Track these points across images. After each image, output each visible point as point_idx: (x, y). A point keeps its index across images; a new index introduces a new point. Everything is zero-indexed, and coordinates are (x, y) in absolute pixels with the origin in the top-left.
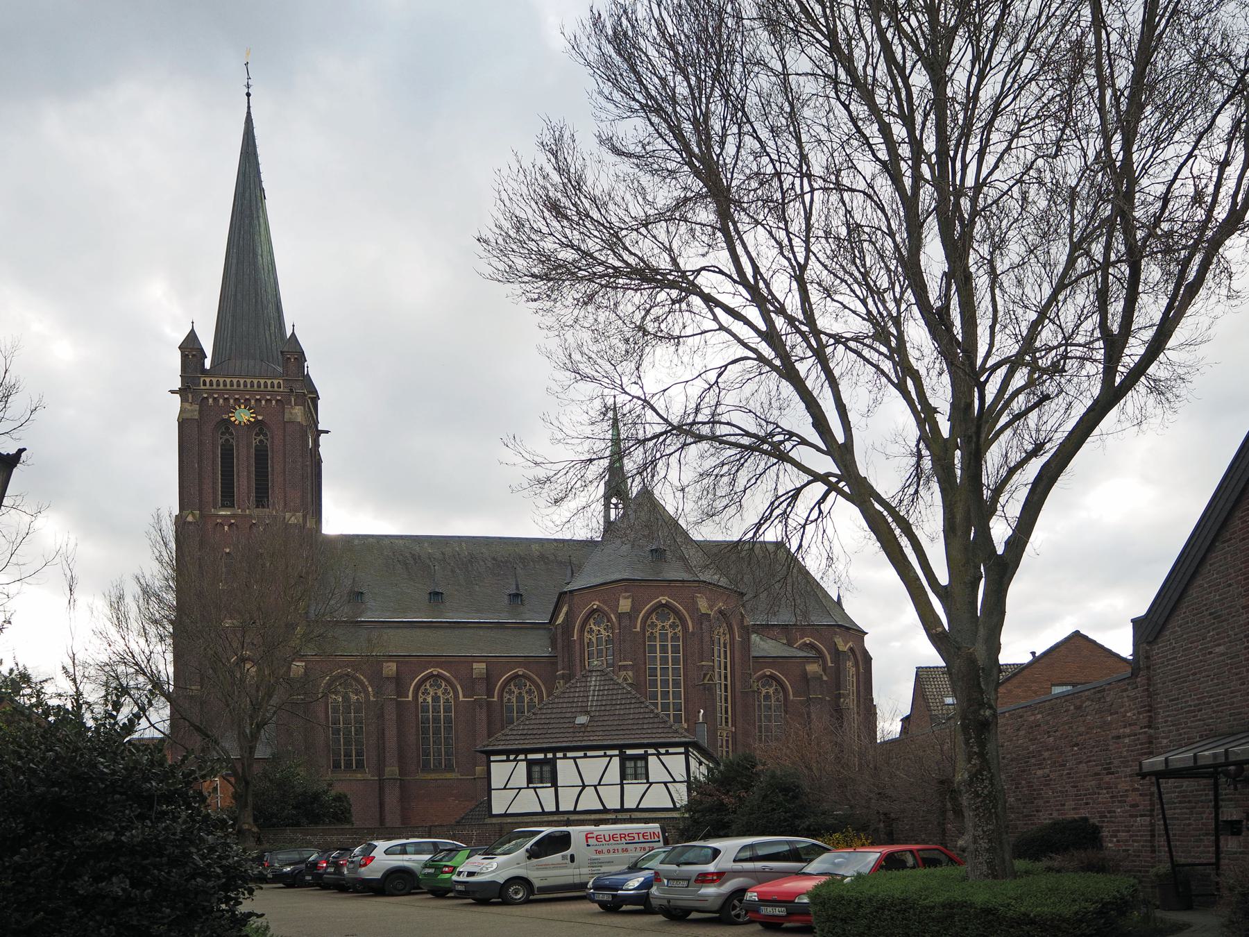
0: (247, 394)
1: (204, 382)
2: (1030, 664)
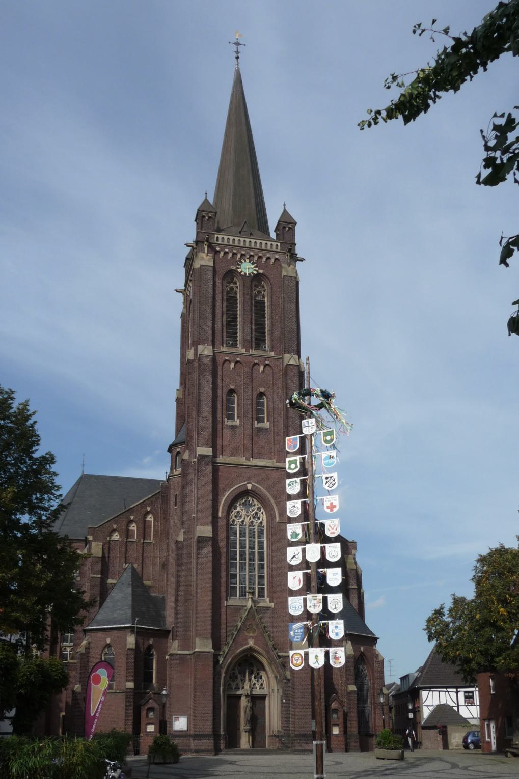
0: (244, 250)
1: (218, 238)
2: (13, 726)
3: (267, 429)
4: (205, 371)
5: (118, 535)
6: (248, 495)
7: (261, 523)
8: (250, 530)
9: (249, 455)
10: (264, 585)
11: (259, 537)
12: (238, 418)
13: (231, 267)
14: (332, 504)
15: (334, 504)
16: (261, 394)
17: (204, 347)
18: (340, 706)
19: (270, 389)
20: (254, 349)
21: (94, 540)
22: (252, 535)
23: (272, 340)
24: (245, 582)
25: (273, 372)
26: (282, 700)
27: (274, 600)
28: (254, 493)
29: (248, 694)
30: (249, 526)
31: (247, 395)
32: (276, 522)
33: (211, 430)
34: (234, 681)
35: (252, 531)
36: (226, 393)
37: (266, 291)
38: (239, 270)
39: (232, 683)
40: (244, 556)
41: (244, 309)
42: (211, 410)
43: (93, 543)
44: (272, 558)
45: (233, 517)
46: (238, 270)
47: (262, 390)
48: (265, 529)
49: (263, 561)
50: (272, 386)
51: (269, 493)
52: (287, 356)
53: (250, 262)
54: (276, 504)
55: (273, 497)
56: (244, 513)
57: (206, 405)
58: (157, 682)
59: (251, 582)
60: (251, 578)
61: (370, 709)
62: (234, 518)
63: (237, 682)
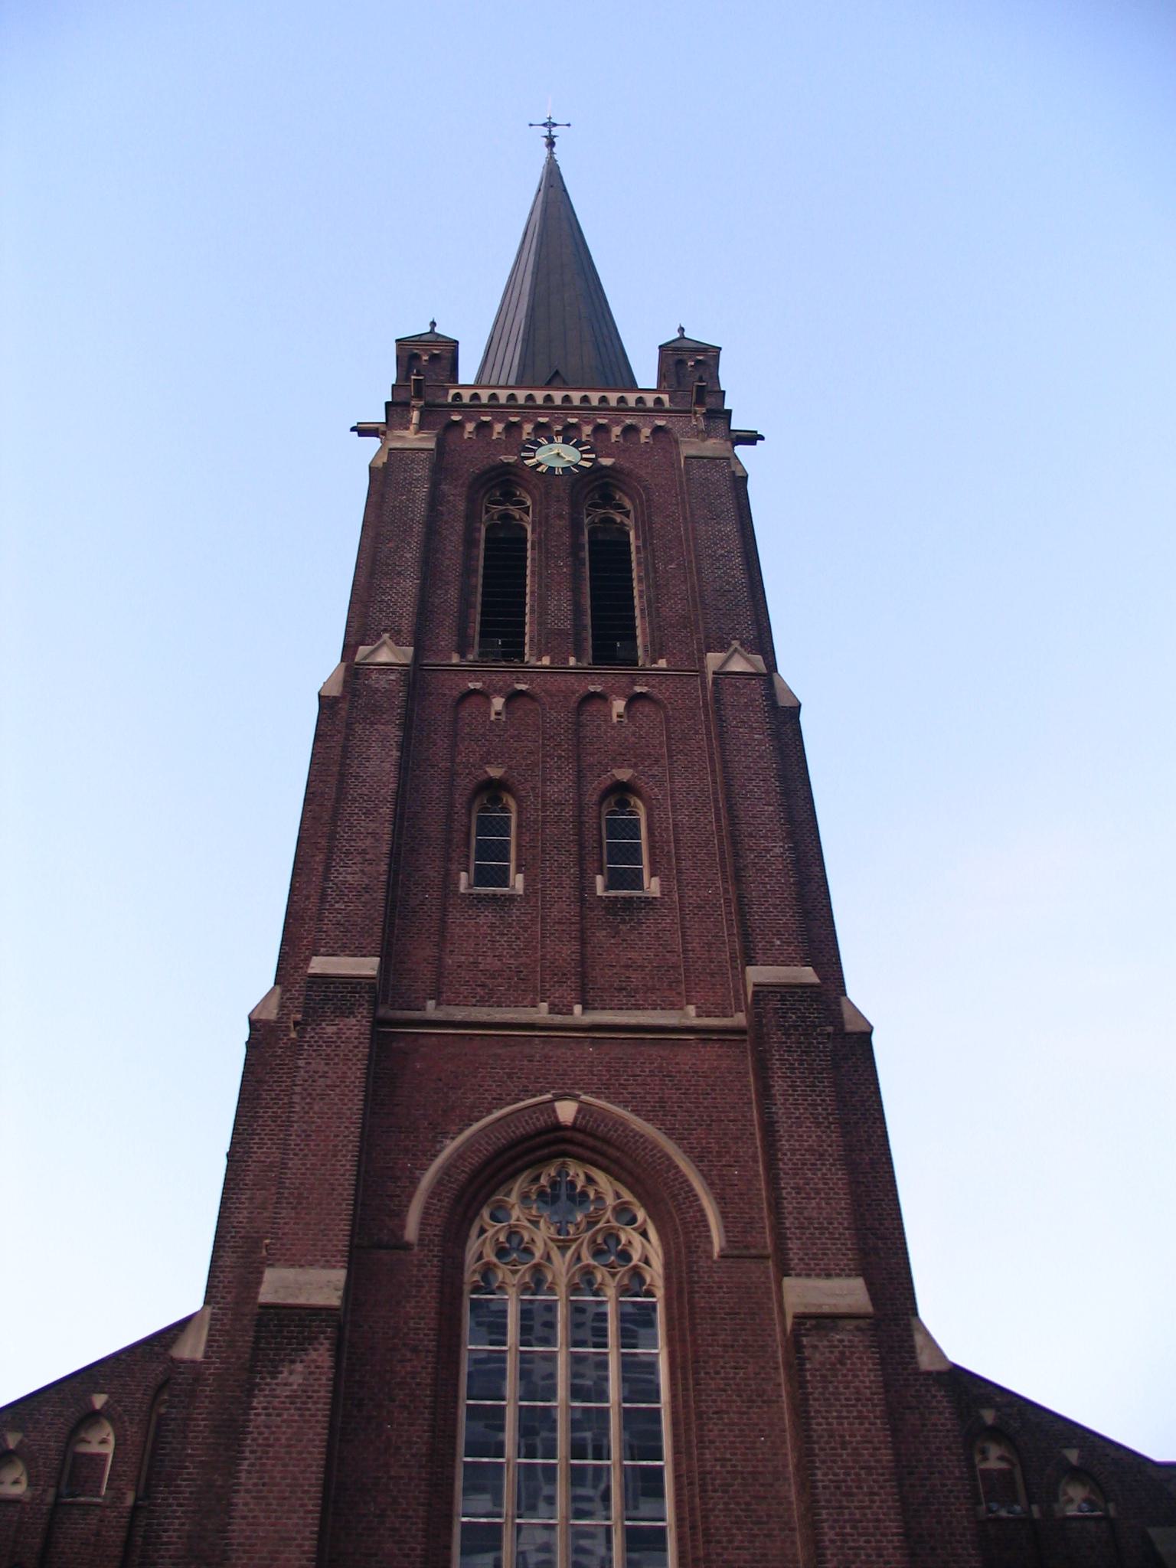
3: (649, 902)
5: (24, 1479)
6: (564, 1154)
8: (577, 1309)
11: (628, 1338)
12: (518, 871)
13: (502, 457)
16: (621, 792)
28: (590, 1141)
30: (574, 1289)
31: (560, 788)
32: (710, 1257)
33: (380, 895)
35: (588, 1317)
37: (632, 514)
40: (544, 1434)
42: (388, 828)
46: (527, 462)
47: (624, 774)
48: (659, 1298)
50: (665, 762)
51: (670, 1133)
54: (705, 1177)
55: (688, 1151)
56: (541, 1236)
57: (368, 813)
60: (583, 1542)
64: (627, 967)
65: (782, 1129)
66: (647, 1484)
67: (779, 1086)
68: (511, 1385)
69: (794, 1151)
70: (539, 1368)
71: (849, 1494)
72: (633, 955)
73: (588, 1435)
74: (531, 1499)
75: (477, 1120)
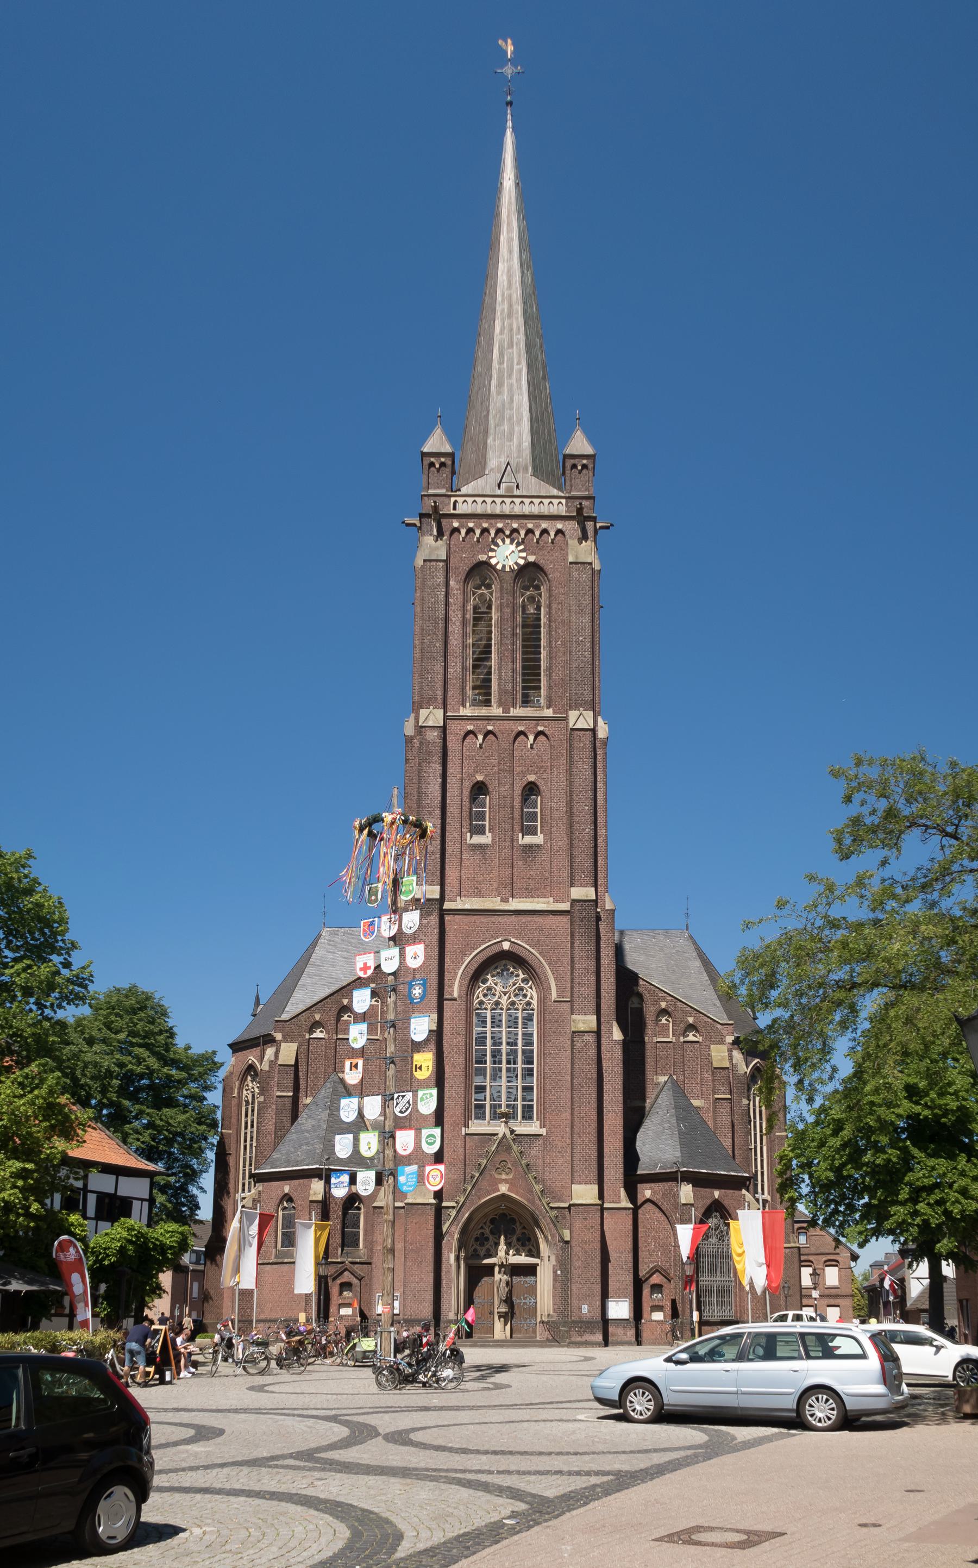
3: (538, 846)
4: (429, 755)
7: (529, 1004)
9: (506, 892)
10: (532, 1101)
11: (525, 1025)
14: (365, 964)
15: (368, 965)
17: (428, 711)
18: (665, 1280)
19: (545, 775)
20: (518, 706)
21: (285, 1039)
22: (513, 1023)
23: (550, 688)
24: (500, 1097)
25: (551, 745)
26: (555, 1272)
27: (547, 1123)
29: (502, 1263)
34: (482, 1245)
35: (513, 1017)
36: (469, 789)
38: (493, 561)
39: (478, 1248)
40: (498, 1057)
41: (501, 634)
43: (283, 1045)
44: (544, 1059)
45: (481, 995)
49: (532, 1063)
52: (573, 715)
53: (511, 543)
58: (365, 1247)
59: (511, 1096)
60: (510, 1090)
61: (733, 1284)
62: (482, 998)
63: (487, 1247)
64: (529, 878)
65: (576, 959)
66: (529, 1073)
67: (577, 943)
68: (489, 1041)
69: (579, 969)
70: (498, 1018)
71: (582, 1087)
72: (532, 873)
73: (512, 1057)
74: (496, 1075)
75: (476, 949)
